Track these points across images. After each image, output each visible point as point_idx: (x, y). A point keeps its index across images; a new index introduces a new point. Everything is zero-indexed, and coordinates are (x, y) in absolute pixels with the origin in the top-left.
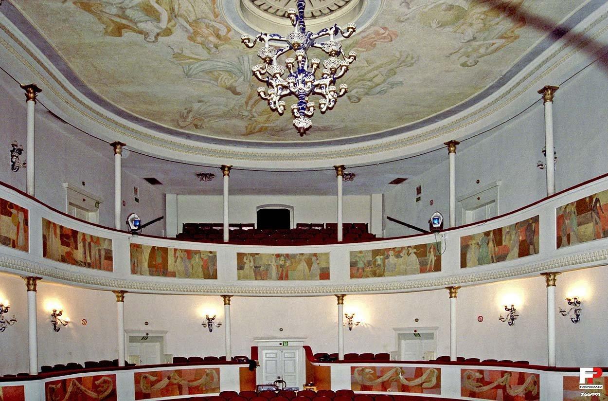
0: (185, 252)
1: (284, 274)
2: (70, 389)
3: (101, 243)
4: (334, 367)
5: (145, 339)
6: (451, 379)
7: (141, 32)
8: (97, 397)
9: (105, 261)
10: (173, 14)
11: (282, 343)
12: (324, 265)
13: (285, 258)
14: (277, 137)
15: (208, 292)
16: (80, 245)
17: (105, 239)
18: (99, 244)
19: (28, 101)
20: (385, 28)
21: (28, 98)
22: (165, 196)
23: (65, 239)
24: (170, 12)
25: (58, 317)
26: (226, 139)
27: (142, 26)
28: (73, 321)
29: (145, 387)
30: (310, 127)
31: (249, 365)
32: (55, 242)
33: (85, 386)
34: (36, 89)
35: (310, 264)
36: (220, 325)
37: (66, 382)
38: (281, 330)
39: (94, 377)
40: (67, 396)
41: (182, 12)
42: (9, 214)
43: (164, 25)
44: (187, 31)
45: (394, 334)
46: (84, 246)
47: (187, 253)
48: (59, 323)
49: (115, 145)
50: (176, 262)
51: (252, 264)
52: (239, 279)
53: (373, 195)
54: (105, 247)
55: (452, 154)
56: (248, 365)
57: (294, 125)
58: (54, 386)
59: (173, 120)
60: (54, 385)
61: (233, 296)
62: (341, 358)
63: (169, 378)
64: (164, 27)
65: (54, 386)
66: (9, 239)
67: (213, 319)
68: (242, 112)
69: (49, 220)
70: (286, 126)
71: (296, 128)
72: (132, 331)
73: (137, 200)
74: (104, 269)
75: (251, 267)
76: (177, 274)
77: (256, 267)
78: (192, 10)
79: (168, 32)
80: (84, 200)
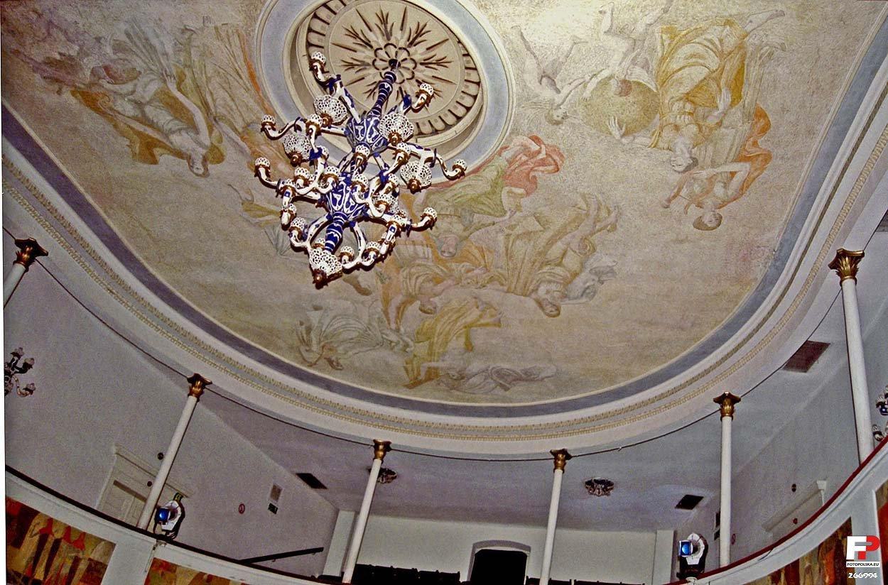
3: (86, 546)
7: (179, 154)
10: (213, 120)
18: (82, 548)
20: (536, 139)
22: (339, 510)
24: (203, 109)
41: (221, 110)
44: (242, 151)
53: (658, 532)
54: (91, 557)
55: (727, 419)
59: (291, 348)
64: (207, 143)
68: (387, 335)
73: (273, 509)
78: (231, 103)
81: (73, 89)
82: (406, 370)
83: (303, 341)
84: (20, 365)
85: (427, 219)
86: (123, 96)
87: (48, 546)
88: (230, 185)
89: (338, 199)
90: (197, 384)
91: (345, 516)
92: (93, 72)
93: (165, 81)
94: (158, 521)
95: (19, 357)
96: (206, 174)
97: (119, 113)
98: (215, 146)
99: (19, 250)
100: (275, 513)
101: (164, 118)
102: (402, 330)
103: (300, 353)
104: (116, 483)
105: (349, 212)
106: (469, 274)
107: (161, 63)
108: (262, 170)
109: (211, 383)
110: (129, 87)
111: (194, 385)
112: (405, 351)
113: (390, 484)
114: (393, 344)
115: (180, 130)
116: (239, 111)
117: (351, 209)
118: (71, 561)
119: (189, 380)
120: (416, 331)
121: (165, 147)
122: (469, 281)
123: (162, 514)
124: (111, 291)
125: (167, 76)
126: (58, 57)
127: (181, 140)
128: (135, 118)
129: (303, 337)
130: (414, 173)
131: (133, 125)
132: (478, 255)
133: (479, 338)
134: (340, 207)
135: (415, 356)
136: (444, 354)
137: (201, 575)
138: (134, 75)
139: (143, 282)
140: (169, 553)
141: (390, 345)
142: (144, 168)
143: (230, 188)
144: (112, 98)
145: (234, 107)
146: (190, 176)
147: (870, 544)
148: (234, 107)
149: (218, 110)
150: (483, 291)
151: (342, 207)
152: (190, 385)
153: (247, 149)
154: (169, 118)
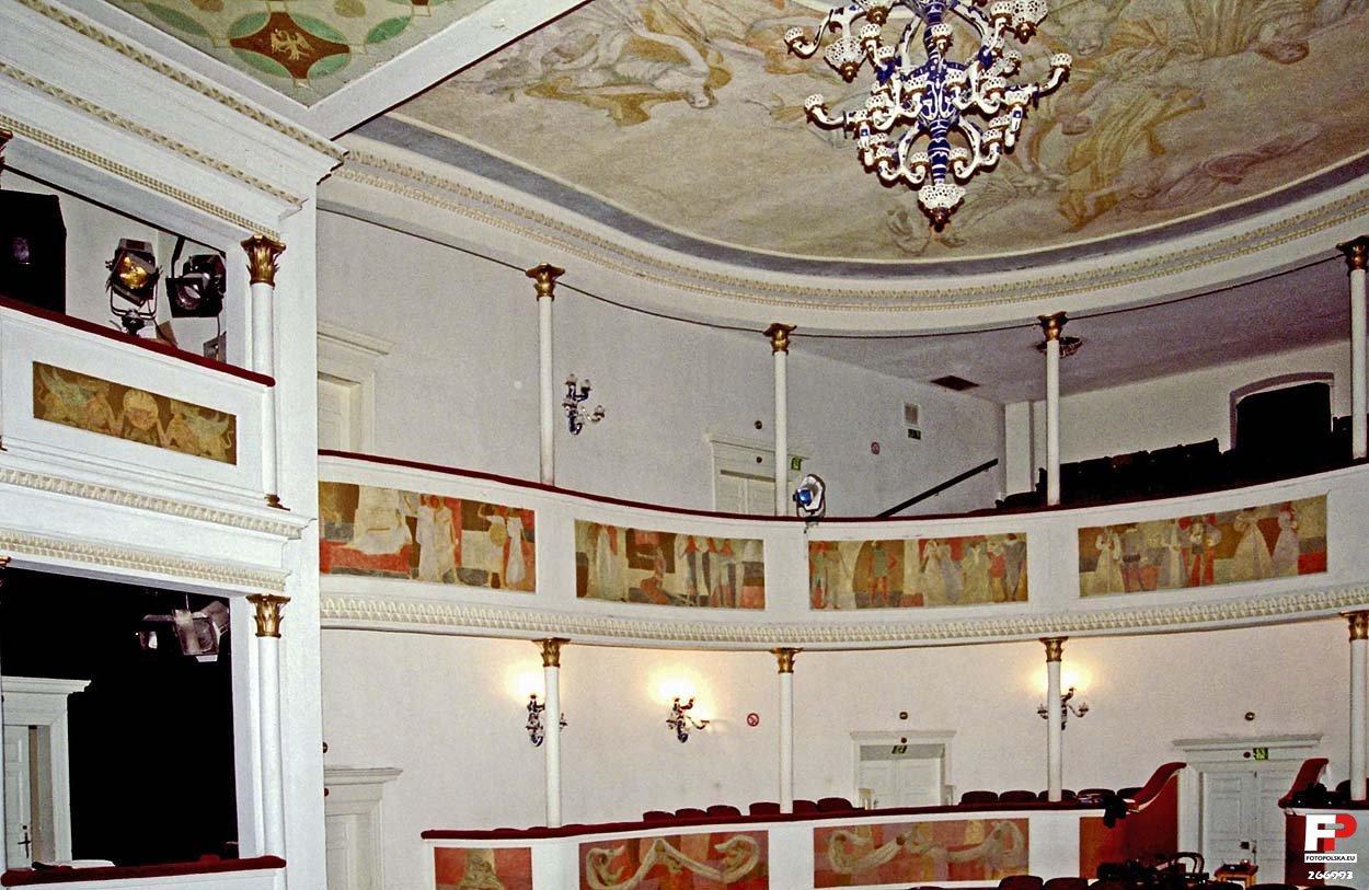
0: (946, 543)
1: (1202, 567)
2: (648, 860)
4: (1036, 818)
5: (900, 750)
6: (554, 866)
7: (673, 97)
8: (718, 878)
9: (746, 588)
10: (703, 41)
11: (1251, 752)
12: (1309, 531)
13: (1205, 527)
14: (1158, 212)
15: (1011, 635)
16: (681, 564)
17: (745, 541)
18: (732, 553)
19: (541, 299)
21: (541, 293)
23: (639, 555)
24: (688, 36)
25: (686, 713)
26: (1033, 251)
27: (665, 84)
28: (724, 718)
29: (840, 862)
30: (962, 201)
31: (1104, 811)
32: (612, 566)
33: (688, 853)
34: (553, 272)
35: (1270, 530)
36: (1084, 710)
37: (638, 844)
38: (1249, 717)
39: (713, 835)
40: (641, 872)
42: (486, 526)
43: (701, 66)
44: (753, 58)
45: (852, 749)
46: (692, 564)
47: (952, 546)
48: (688, 723)
49: (772, 331)
50: (923, 569)
51: (1117, 552)
52: (1084, 594)
54: (745, 559)
56: (1101, 813)
57: (921, 205)
58: (606, 852)
60: (606, 848)
61: (800, 650)
62: (787, 809)
63: (900, 841)
64: (704, 68)
65: (606, 852)
66: (485, 574)
67: (689, 707)
68: (1021, 182)
69: (595, 521)
70: (1158, 179)
71: (926, 212)
72: (867, 735)
73: (914, 434)
74: (743, 606)
75: (1115, 561)
76: (925, 598)
77: (1127, 559)
78: (722, 14)
79: (721, 77)
80: (759, 460)
81: (526, 88)
82: (1063, 213)
83: (899, 232)
84: (579, 392)
85: (1059, 72)
86: (585, 69)
87: (699, 562)
88: (748, 101)
89: (930, 106)
90: (778, 334)
91: (1016, 412)
92: (543, 61)
93: (631, 30)
94: (800, 504)
95: (574, 384)
96: (713, 102)
97: (586, 88)
98: (716, 68)
99: (535, 281)
100: (919, 438)
101: (641, 68)
102: (1042, 167)
103: (899, 246)
104: (723, 472)
105: (950, 114)
106: (1133, 61)
107: (619, 14)
108: (818, 112)
109: (795, 327)
110: (590, 57)
111: (775, 339)
112: (1055, 191)
113: (1075, 355)
114: (1034, 189)
115: (665, 72)
116: (735, 17)
117: (950, 111)
118: (727, 569)
119: (767, 334)
120: (1065, 161)
121: (653, 97)
122: (1134, 70)
123: (801, 499)
124: (641, 275)
125: (631, 22)
126: (500, 66)
127: (674, 80)
128: (607, 85)
129: (897, 227)
130: (1020, 15)
131: (606, 93)
132: (1141, 32)
133: (1171, 135)
134: (935, 115)
135: (1071, 191)
136: (1117, 174)
137: (867, 544)
138: (592, 42)
139: (668, 246)
140: (823, 532)
141: (1031, 192)
142: (635, 131)
143: (749, 104)
144: (573, 77)
145: (726, 16)
146: (694, 114)
147: (1341, 826)
148: (726, 16)
149: (707, 29)
150: (1164, 73)
151: (939, 113)
152: (771, 339)
153: (759, 53)
154: (648, 65)
